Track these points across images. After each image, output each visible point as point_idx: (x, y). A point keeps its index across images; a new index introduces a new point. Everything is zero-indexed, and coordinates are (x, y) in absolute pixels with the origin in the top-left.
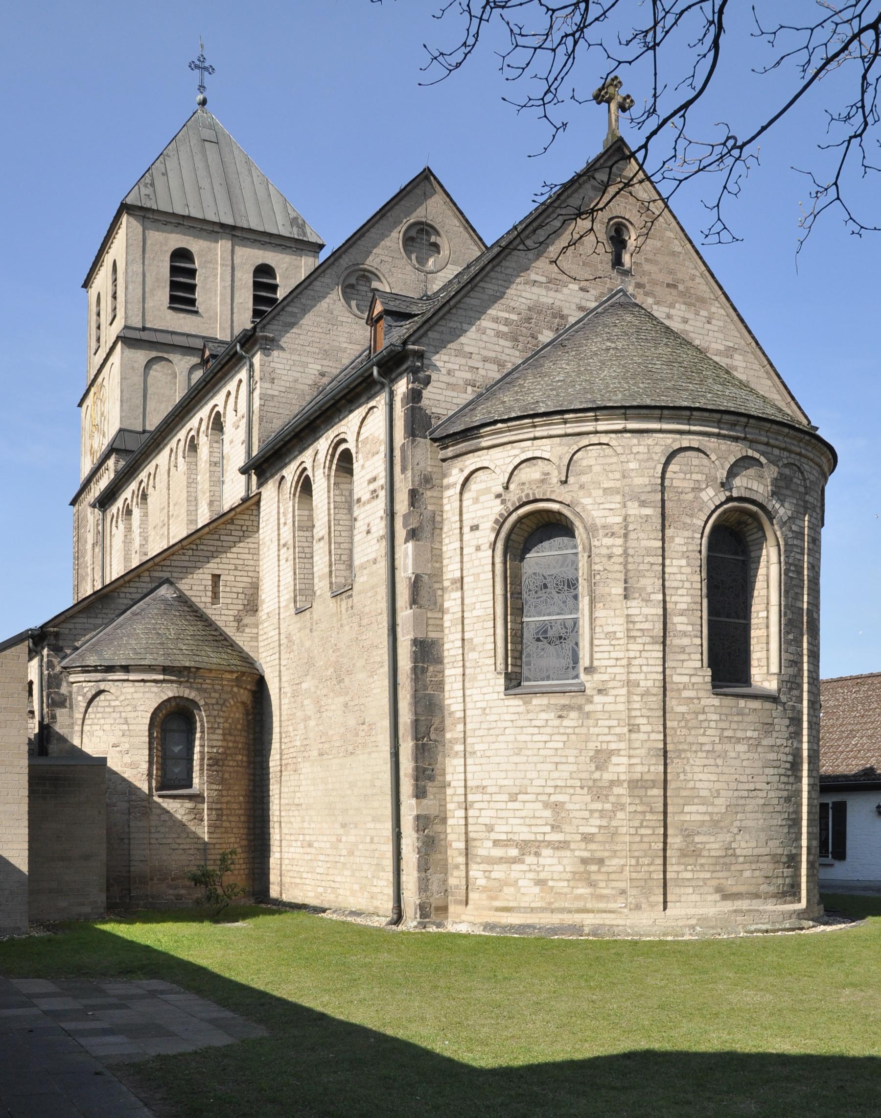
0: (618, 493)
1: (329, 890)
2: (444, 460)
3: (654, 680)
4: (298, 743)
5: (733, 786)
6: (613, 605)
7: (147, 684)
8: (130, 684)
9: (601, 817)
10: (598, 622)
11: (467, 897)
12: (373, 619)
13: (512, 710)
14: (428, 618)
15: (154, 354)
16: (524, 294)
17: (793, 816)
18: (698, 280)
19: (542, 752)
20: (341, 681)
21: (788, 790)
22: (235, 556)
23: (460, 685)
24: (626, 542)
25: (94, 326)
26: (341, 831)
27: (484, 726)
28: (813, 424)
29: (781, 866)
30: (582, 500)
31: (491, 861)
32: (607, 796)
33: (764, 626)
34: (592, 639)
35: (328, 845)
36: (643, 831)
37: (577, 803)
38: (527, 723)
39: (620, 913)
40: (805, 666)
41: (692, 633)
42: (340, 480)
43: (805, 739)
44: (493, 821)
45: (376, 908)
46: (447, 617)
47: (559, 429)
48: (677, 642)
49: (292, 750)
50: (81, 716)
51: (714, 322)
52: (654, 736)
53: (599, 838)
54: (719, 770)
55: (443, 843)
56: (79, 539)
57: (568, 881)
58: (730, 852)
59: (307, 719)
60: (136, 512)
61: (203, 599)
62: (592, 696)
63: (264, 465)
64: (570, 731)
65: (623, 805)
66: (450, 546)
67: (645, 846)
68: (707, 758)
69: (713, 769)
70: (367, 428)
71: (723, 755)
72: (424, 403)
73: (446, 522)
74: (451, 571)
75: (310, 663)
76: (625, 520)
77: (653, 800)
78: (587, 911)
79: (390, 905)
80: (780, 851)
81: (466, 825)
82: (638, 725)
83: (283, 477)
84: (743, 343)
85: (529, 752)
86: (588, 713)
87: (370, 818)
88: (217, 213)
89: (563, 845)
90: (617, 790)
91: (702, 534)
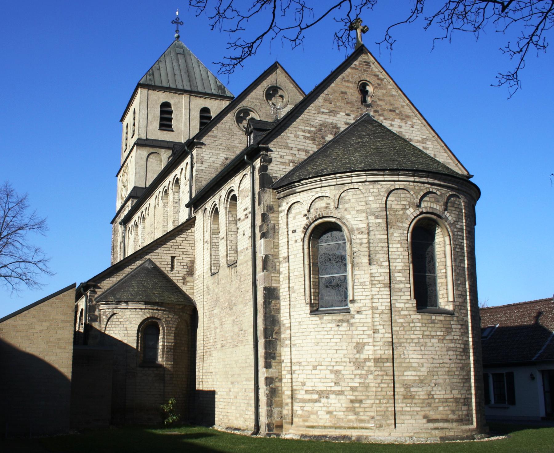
0: (364, 212)
1: (225, 417)
2: (279, 199)
3: (386, 306)
4: (212, 341)
5: (431, 361)
6: (364, 268)
7: (137, 310)
8: (129, 311)
9: (360, 378)
10: (356, 277)
11: (292, 420)
12: (246, 278)
13: (313, 322)
14: (272, 277)
15: (152, 150)
16: (318, 118)
17: (466, 377)
18: (406, 107)
19: (329, 344)
20: (231, 309)
21: (462, 363)
22: (183, 247)
23: (288, 310)
24: (369, 236)
25: (124, 139)
26: (231, 386)
27: (301, 331)
28: (471, 174)
29: (460, 404)
30: (346, 216)
31: (304, 401)
32: (363, 367)
33: (444, 277)
34: (353, 286)
35: (225, 393)
36: (382, 385)
37: (348, 371)
38: (321, 329)
39: (371, 429)
40: (468, 297)
41: (405, 282)
42: (231, 209)
43: (470, 336)
44: (305, 380)
45: (247, 426)
46: (281, 276)
47: (333, 182)
48: (397, 286)
49: (209, 344)
50: (104, 326)
51: (415, 126)
52: (386, 335)
53: (360, 389)
54: (422, 353)
55: (280, 392)
56: (114, 240)
57: (344, 412)
58: (431, 396)
59: (216, 328)
60: (140, 226)
61: (167, 269)
62: (354, 315)
63: (196, 203)
64: (343, 333)
65: (372, 371)
66: (282, 240)
67: (384, 393)
68: (416, 346)
69: (419, 352)
70: (243, 184)
71: (424, 344)
72: (269, 171)
73: (280, 229)
74: (283, 253)
75: (218, 300)
76: (368, 225)
77: (387, 369)
78: (354, 428)
79: (253, 424)
80: (459, 396)
81: (292, 382)
82: (378, 329)
83: (206, 209)
84: (431, 136)
85: (323, 344)
86: (352, 324)
87: (244, 379)
88: (183, 86)
89: (341, 393)
90: (368, 364)
91: (408, 231)
